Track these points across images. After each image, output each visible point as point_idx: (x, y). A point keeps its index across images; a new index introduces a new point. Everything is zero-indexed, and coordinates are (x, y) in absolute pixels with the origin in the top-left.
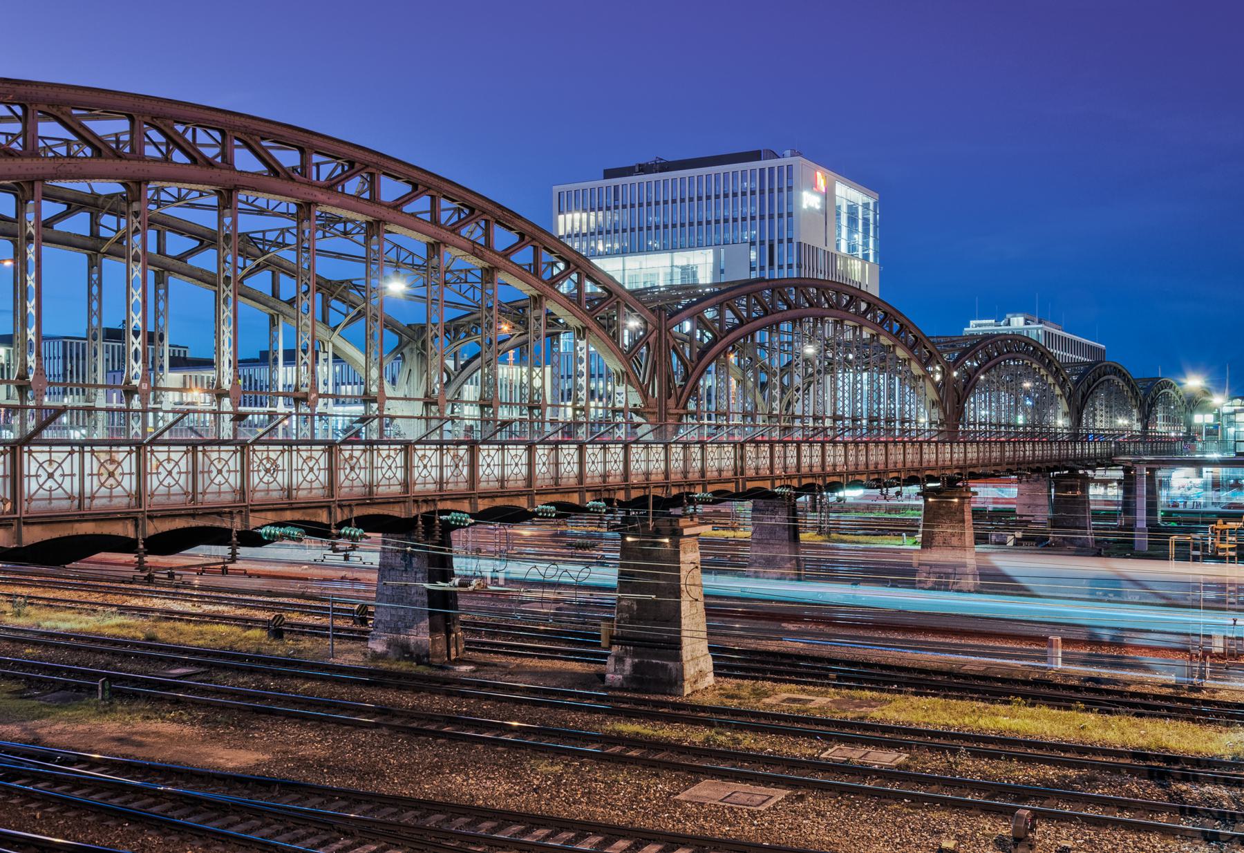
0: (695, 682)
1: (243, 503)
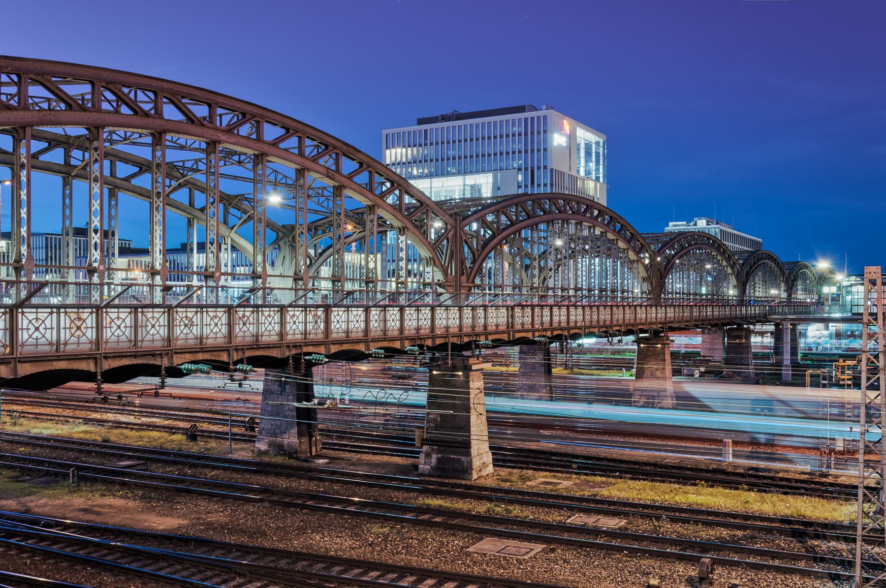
0: (480, 471)
1: (169, 348)
